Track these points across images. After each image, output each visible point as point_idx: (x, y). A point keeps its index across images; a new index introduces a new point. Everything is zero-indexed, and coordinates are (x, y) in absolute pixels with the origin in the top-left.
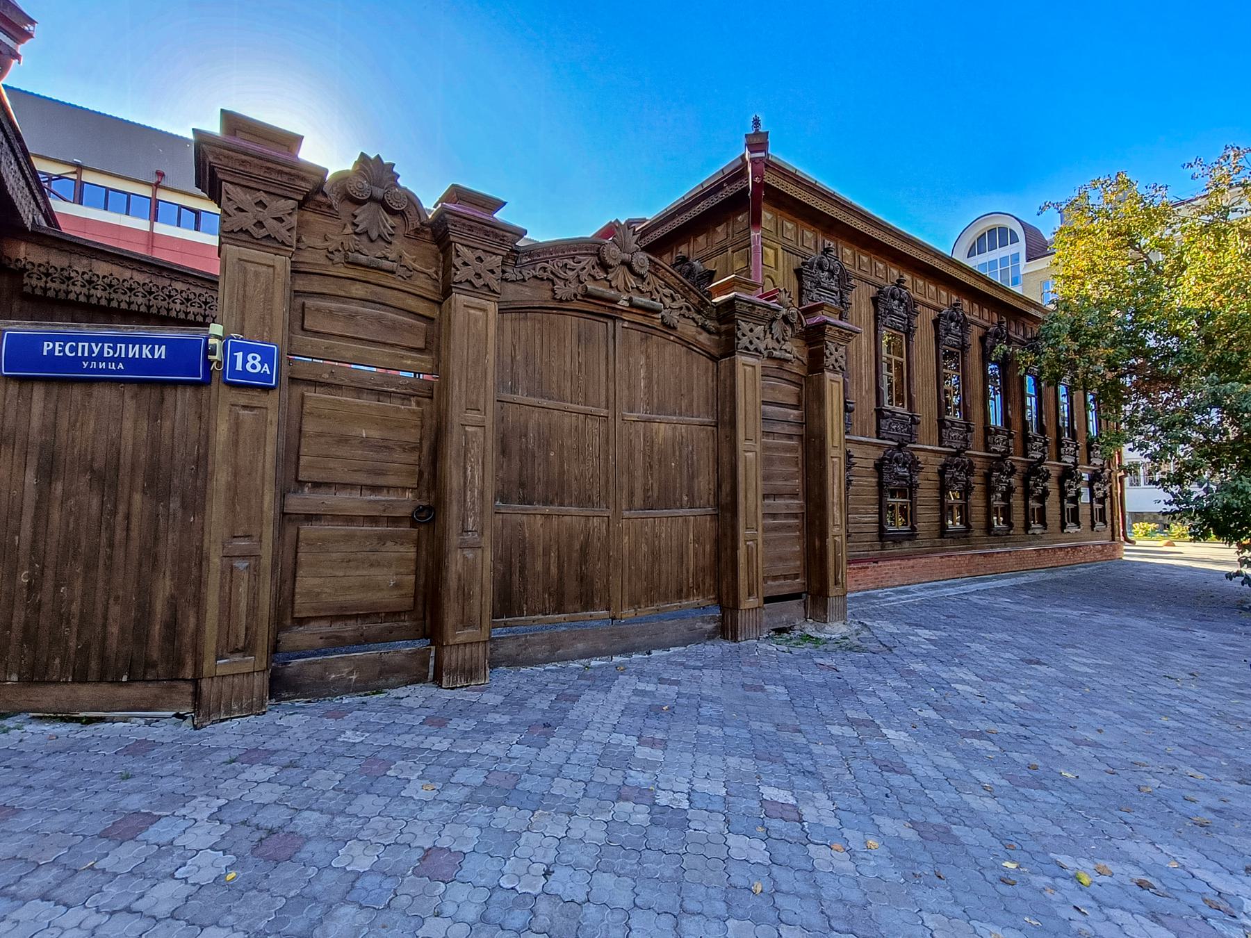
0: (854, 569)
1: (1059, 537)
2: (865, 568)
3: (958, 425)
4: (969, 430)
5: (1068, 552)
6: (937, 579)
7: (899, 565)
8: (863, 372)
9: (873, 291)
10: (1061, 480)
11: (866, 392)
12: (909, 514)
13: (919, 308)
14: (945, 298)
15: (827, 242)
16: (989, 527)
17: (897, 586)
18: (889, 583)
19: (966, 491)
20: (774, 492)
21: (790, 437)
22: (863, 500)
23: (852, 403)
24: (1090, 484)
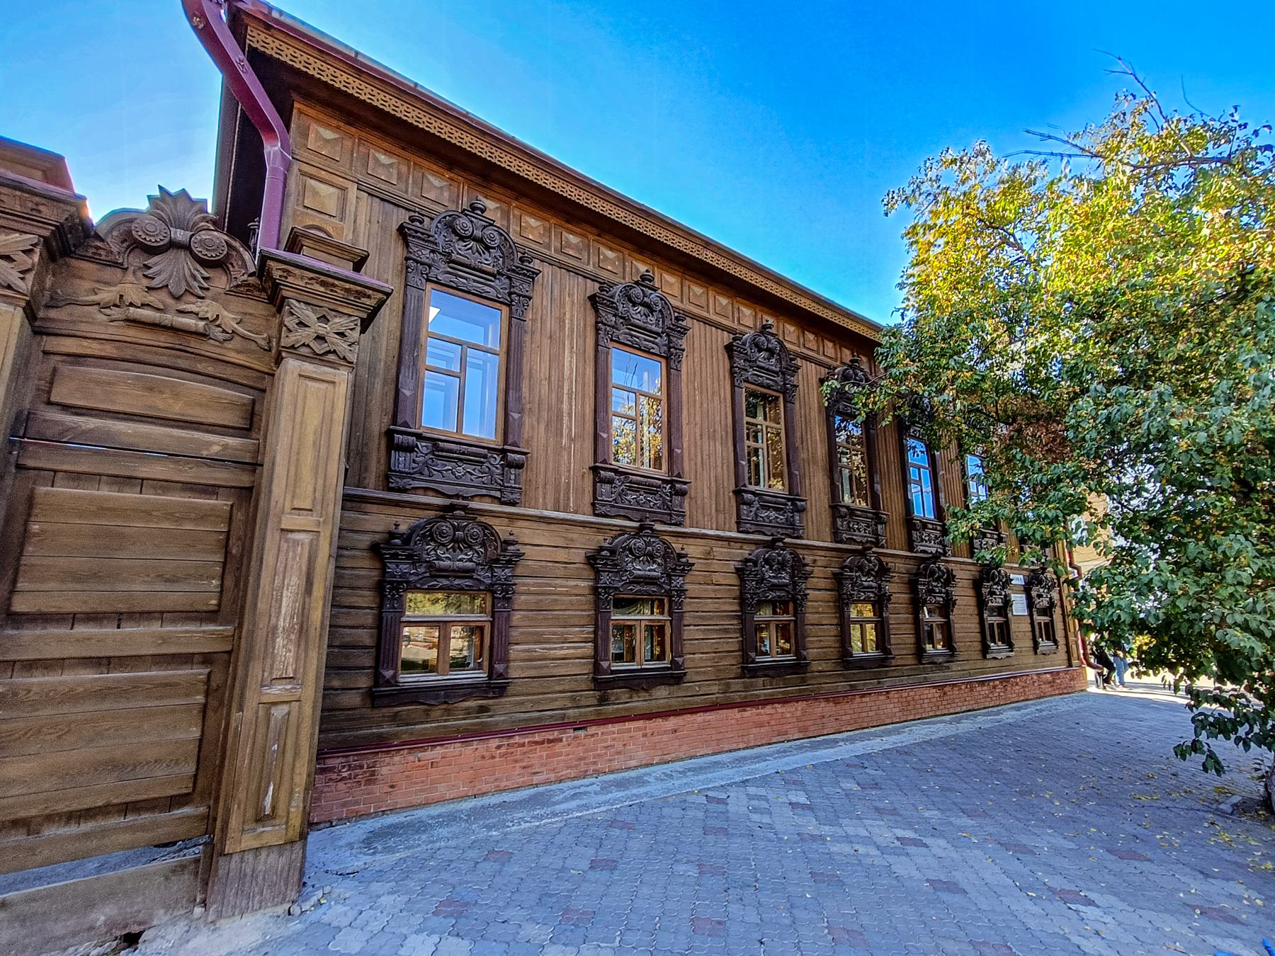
0: (523, 745)
1: (980, 664)
2: (550, 741)
3: (930, 526)
4: (878, 519)
5: (994, 687)
6: (734, 746)
7: (639, 729)
8: (565, 406)
9: (726, 338)
10: (977, 585)
11: (571, 440)
12: (793, 633)
13: (687, 322)
14: (747, 318)
15: (766, 317)
16: (919, 652)
17: (636, 767)
18: (615, 764)
19: (880, 602)
20: (122, 607)
21: (209, 490)
22: (556, 618)
23: (803, 501)
24: (1027, 589)
